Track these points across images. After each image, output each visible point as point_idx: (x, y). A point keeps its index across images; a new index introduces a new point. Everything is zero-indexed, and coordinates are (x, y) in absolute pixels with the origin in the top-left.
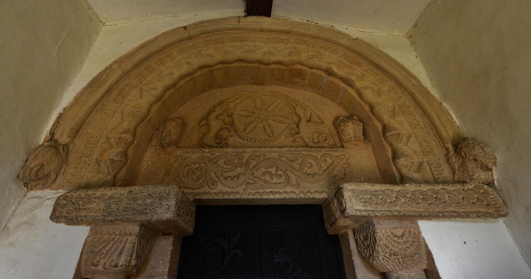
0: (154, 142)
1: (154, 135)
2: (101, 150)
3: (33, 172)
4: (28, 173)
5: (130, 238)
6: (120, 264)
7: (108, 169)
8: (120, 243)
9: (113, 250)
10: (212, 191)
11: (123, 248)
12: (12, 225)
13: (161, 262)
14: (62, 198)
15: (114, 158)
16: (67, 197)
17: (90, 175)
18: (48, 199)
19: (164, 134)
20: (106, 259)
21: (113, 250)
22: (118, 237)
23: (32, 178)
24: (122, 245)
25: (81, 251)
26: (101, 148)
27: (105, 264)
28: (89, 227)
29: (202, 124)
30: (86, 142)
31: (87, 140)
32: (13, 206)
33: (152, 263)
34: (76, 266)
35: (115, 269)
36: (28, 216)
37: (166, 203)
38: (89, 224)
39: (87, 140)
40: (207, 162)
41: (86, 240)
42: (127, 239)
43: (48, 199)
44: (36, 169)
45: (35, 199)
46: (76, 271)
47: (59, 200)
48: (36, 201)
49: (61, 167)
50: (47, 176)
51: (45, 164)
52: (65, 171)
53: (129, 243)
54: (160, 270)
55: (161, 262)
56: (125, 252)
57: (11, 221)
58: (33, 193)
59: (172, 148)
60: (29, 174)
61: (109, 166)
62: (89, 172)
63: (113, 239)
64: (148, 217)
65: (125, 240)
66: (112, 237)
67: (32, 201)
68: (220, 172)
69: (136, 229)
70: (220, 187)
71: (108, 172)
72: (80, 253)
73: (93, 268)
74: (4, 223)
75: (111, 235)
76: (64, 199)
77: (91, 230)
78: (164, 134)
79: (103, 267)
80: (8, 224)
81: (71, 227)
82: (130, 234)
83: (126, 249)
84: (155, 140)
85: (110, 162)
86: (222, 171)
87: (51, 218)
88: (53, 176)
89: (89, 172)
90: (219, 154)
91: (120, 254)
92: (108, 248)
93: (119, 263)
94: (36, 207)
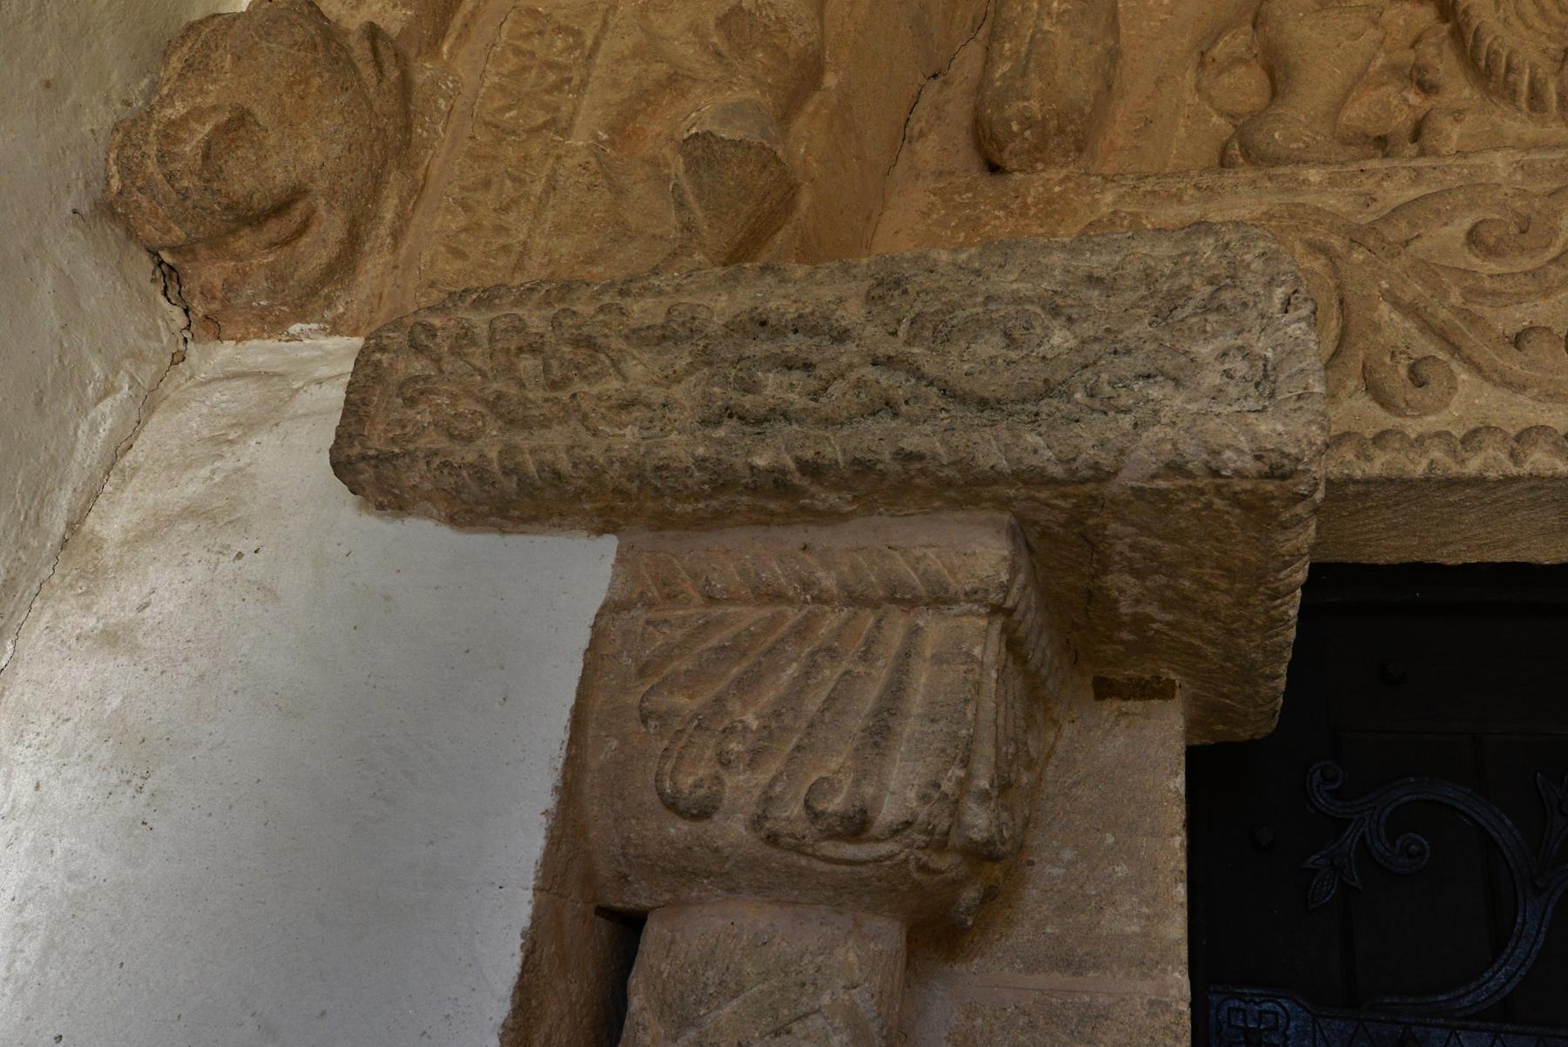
0: (927, 151)
1: (923, 110)
2: (615, 97)
3: (190, 148)
4: (152, 150)
5: (934, 628)
6: (888, 813)
7: (681, 205)
8: (866, 657)
9: (812, 704)
10: (1413, 428)
11: (896, 690)
12: (112, 522)
13: (1121, 870)
14: (399, 338)
15: (714, 128)
16: (431, 332)
17: (565, 247)
18: (319, 382)
19: (1004, 68)
20: (774, 766)
21: (812, 704)
22: (831, 621)
23: (206, 234)
24: (881, 672)
25: (570, 699)
26: (616, 84)
27: (767, 799)
28: (610, 543)
29: (1220, 51)
30: (513, 62)
31: (518, 52)
32: (106, 406)
33: (1058, 871)
34: (549, 801)
35: (849, 850)
36: (204, 472)
37: (1227, 340)
38: (605, 523)
39: (518, 52)
40: (1336, 242)
41: (593, 655)
42: (915, 631)
43: (319, 382)
44: (203, 130)
45: (235, 383)
46: (555, 840)
47: (383, 349)
48: (251, 392)
49: (377, 181)
50: (281, 210)
51: (262, 114)
52: (403, 217)
53: (938, 659)
54: (1124, 920)
55: (1121, 870)
56: (909, 727)
57: (102, 500)
58: (225, 352)
59: (1055, 174)
60: (161, 158)
61: (687, 186)
62: (560, 230)
63: (802, 631)
64: (1089, 440)
65: (895, 634)
66: (793, 615)
67: (219, 395)
68: (1455, 298)
69: (982, 553)
70: (1469, 399)
71: (687, 227)
72: (565, 717)
73: (678, 829)
74: (64, 499)
75: (777, 597)
76: (416, 348)
77: (621, 559)
78: (1004, 68)
79: (756, 823)
80: (91, 520)
81: (482, 544)
82: (940, 599)
83: (916, 702)
84: (932, 136)
85: (693, 164)
86: (1468, 293)
87: (342, 466)
88: (330, 228)
89: (560, 230)
90: (1412, 193)
91: (879, 734)
92: (769, 695)
93: (877, 799)
94: (249, 425)
